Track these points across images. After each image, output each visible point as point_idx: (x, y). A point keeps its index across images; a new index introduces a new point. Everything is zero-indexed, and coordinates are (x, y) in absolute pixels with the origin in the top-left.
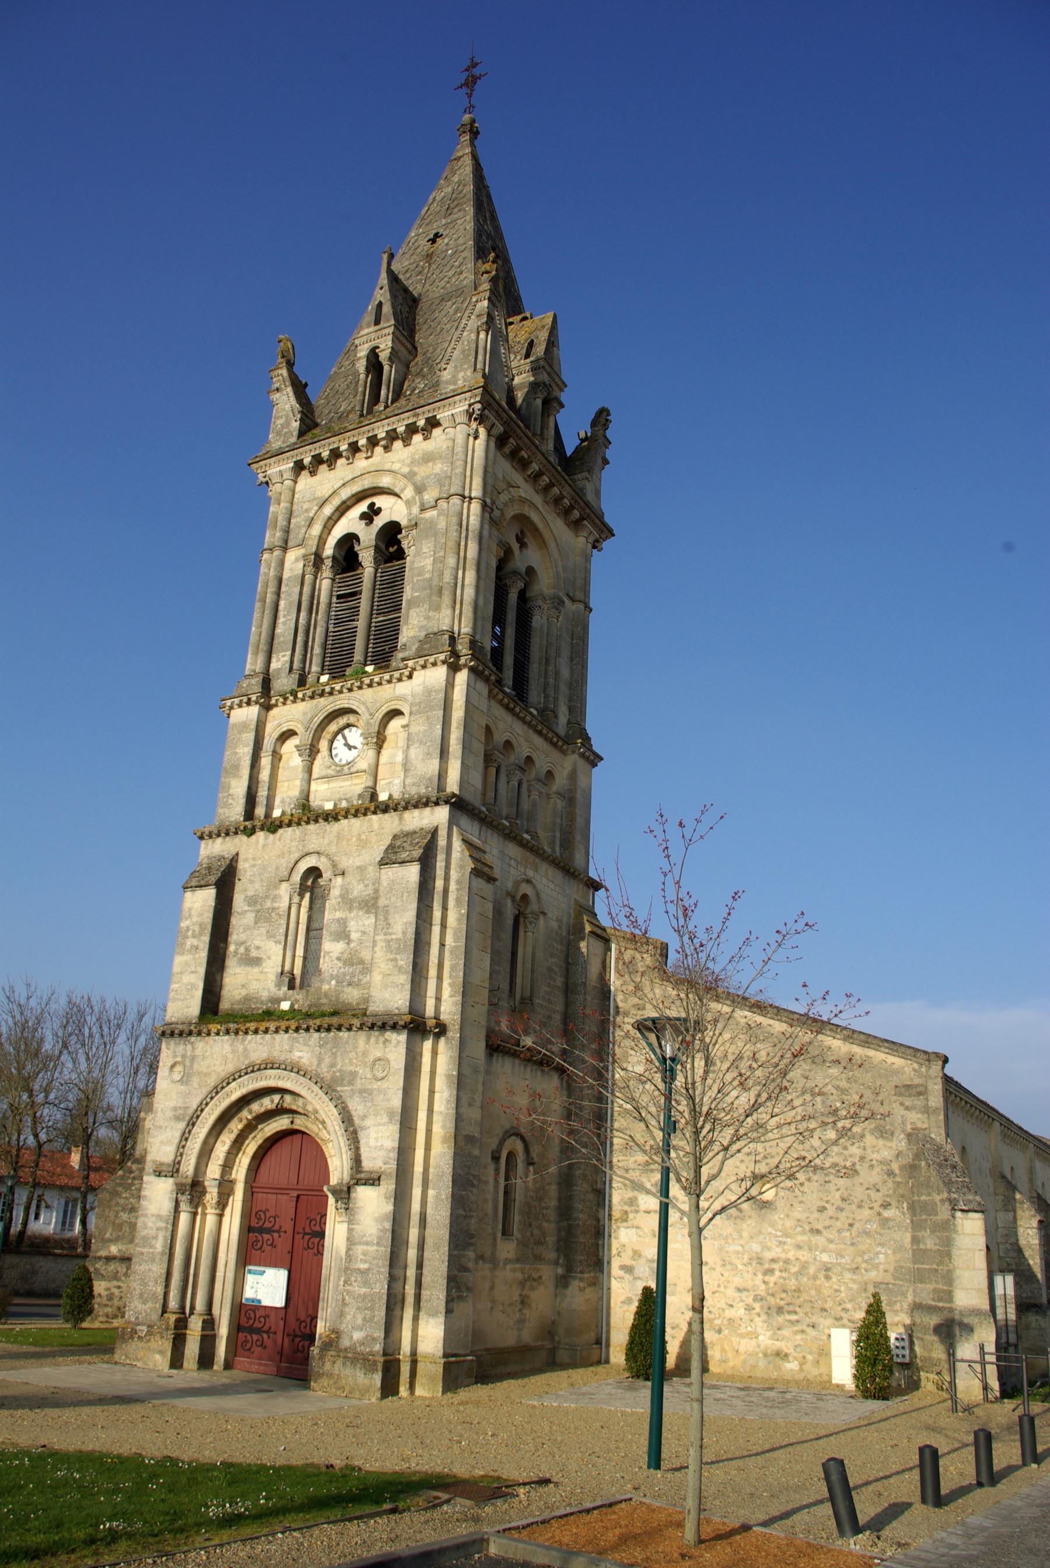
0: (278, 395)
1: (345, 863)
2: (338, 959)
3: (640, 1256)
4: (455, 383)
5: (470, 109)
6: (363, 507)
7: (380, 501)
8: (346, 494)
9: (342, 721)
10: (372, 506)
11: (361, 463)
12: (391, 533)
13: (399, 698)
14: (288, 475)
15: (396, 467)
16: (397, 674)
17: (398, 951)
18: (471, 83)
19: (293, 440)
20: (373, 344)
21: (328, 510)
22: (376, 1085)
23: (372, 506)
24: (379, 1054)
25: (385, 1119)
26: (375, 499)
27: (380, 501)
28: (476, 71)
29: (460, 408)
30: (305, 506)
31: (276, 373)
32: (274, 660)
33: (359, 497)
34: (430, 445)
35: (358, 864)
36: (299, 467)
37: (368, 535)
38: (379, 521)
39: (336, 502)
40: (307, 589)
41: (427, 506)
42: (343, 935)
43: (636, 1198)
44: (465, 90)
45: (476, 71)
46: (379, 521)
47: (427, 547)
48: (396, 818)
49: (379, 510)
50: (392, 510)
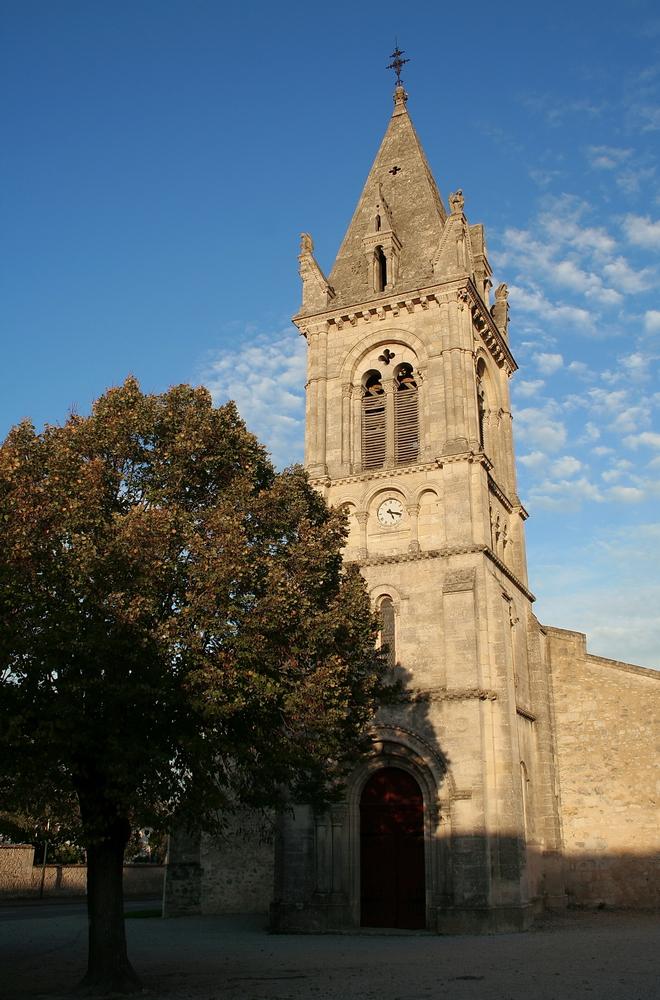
0: (307, 274)
1: (408, 591)
2: (413, 654)
3: (588, 835)
4: (445, 274)
5: (399, 82)
6: (380, 351)
7: (392, 349)
8: (368, 343)
9: (393, 494)
10: (387, 351)
11: (376, 323)
12: (405, 369)
13: (434, 481)
14: (323, 329)
15: (405, 327)
16: (421, 468)
17: (465, 648)
18: (398, 65)
19: (324, 305)
20: (378, 243)
21: (356, 354)
22: (460, 735)
23: (387, 351)
24: (459, 715)
25: (470, 757)
26: (390, 347)
27: (392, 349)
28: (402, 57)
29: (453, 290)
30: (338, 350)
31: (303, 259)
32: (328, 454)
33: (377, 345)
34: (428, 314)
35: (419, 591)
36: (331, 322)
37: (387, 372)
38: (395, 362)
39: (362, 349)
40: (346, 407)
41: (433, 354)
42: (412, 638)
43: (582, 799)
44: (393, 70)
45: (402, 57)
46: (395, 362)
47: (438, 381)
48: (445, 562)
49: (393, 355)
50: (402, 356)
